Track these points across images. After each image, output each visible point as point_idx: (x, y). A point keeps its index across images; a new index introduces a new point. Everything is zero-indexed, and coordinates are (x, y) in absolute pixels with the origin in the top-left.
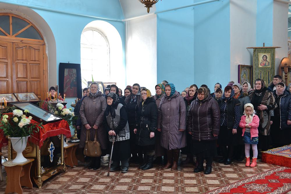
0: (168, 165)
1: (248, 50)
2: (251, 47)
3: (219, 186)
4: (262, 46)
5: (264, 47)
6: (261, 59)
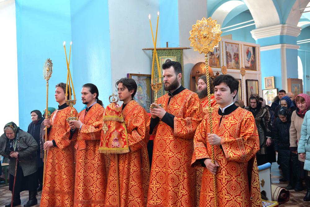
1: (144, 51)
4: (165, 47)
5: (167, 48)
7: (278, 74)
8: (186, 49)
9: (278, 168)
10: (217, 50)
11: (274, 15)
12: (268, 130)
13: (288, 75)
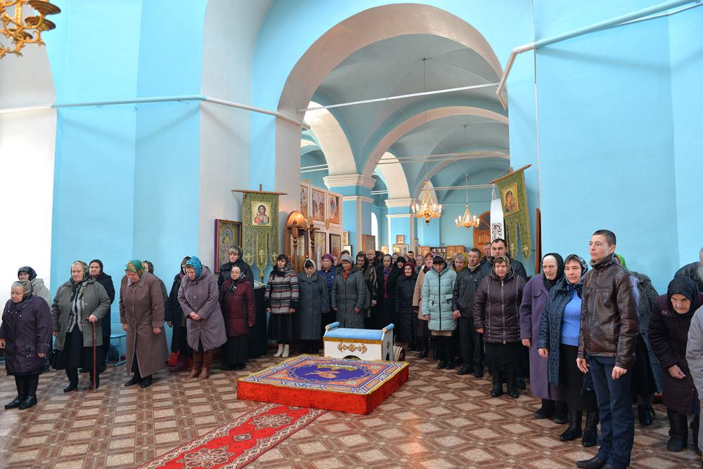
0: (194, 372)
2: (240, 189)
3: (177, 445)
4: (257, 189)
6: (255, 210)
7: (353, 230)
11: (348, 162)
12: (374, 294)
13: (363, 231)
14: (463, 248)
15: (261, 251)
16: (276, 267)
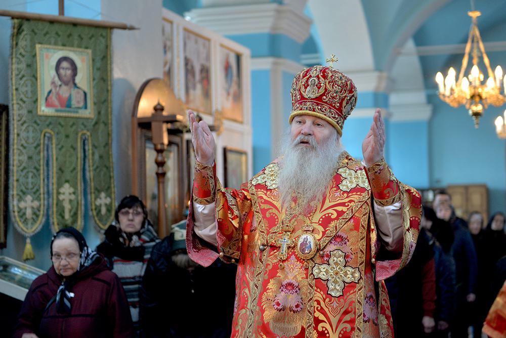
4: (50, 10)
5: (61, 18)
8: (124, 28)
9: (133, 194)
10: (167, 48)
14: (483, 190)
15: (67, 189)
16: (113, 233)
